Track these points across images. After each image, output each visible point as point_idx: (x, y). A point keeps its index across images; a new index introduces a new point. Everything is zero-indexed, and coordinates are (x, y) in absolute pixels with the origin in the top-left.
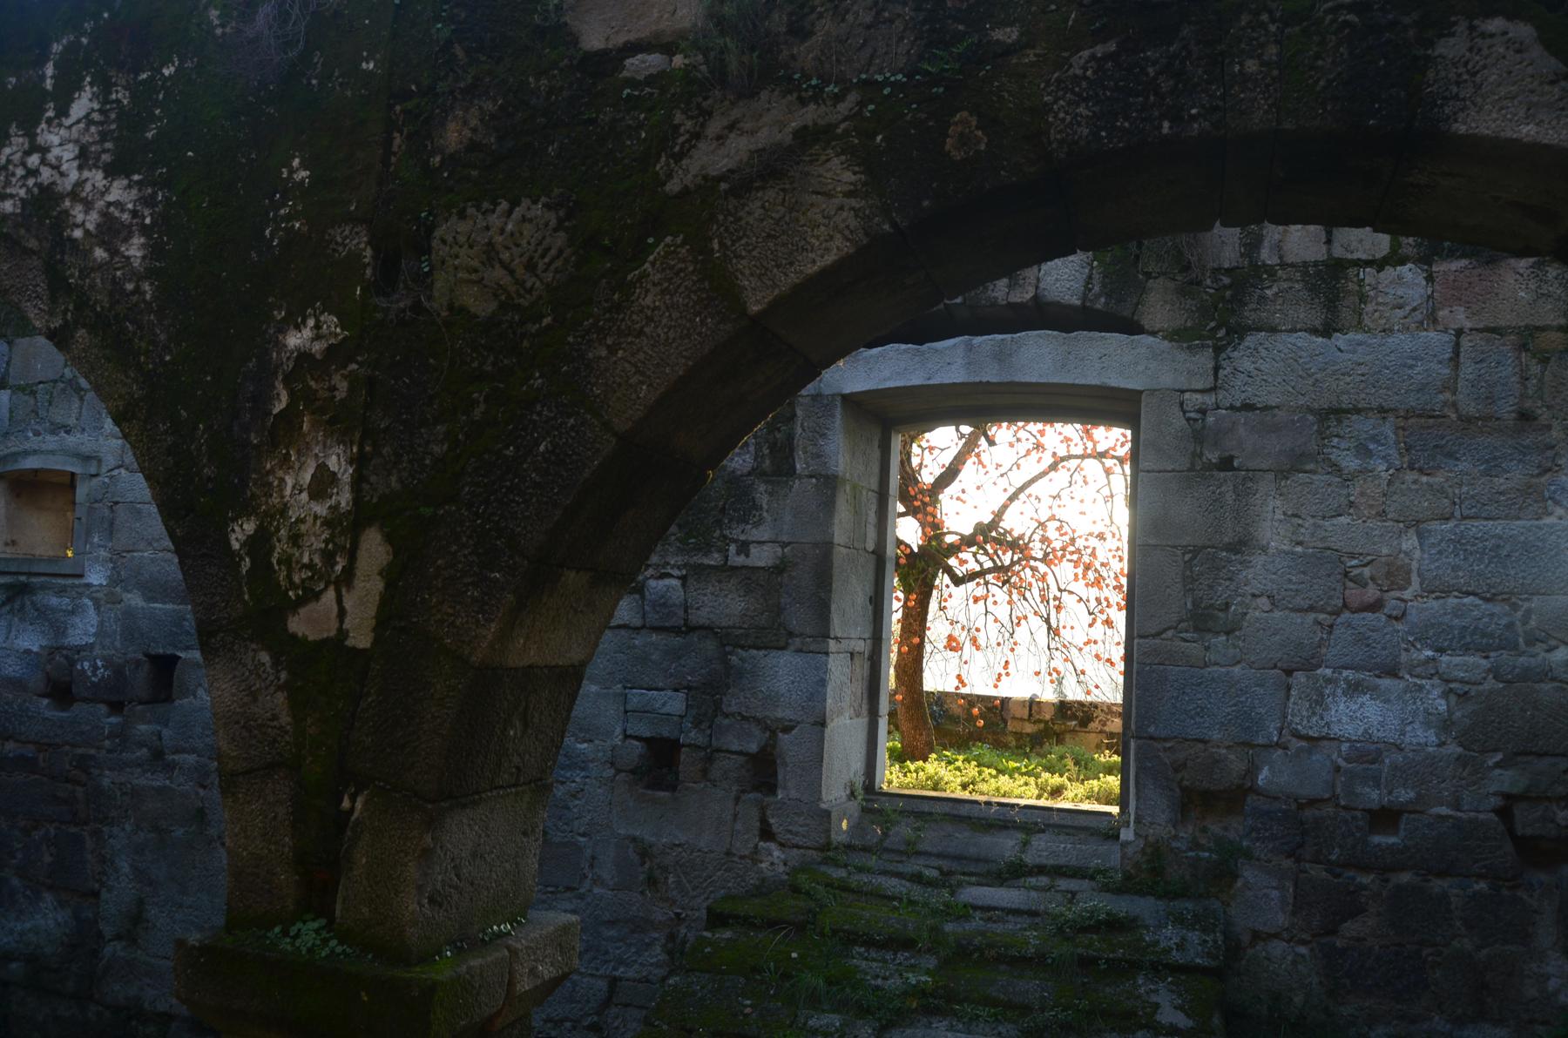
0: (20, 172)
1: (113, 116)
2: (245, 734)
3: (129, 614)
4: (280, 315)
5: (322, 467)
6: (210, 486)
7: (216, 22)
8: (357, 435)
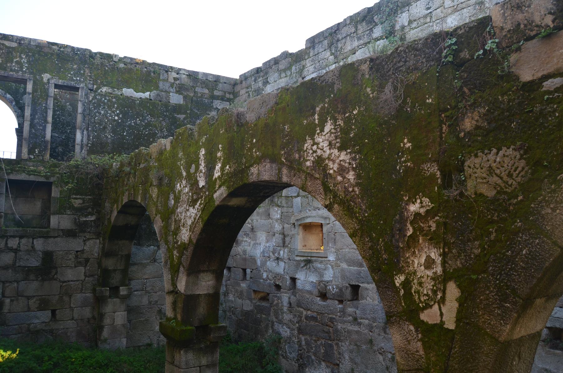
0: (311, 152)
1: (339, 130)
2: (406, 356)
3: (343, 270)
4: (406, 198)
5: (428, 257)
6: (386, 262)
7: (370, 92)
8: (442, 245)
